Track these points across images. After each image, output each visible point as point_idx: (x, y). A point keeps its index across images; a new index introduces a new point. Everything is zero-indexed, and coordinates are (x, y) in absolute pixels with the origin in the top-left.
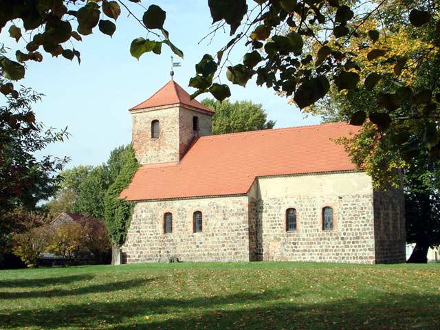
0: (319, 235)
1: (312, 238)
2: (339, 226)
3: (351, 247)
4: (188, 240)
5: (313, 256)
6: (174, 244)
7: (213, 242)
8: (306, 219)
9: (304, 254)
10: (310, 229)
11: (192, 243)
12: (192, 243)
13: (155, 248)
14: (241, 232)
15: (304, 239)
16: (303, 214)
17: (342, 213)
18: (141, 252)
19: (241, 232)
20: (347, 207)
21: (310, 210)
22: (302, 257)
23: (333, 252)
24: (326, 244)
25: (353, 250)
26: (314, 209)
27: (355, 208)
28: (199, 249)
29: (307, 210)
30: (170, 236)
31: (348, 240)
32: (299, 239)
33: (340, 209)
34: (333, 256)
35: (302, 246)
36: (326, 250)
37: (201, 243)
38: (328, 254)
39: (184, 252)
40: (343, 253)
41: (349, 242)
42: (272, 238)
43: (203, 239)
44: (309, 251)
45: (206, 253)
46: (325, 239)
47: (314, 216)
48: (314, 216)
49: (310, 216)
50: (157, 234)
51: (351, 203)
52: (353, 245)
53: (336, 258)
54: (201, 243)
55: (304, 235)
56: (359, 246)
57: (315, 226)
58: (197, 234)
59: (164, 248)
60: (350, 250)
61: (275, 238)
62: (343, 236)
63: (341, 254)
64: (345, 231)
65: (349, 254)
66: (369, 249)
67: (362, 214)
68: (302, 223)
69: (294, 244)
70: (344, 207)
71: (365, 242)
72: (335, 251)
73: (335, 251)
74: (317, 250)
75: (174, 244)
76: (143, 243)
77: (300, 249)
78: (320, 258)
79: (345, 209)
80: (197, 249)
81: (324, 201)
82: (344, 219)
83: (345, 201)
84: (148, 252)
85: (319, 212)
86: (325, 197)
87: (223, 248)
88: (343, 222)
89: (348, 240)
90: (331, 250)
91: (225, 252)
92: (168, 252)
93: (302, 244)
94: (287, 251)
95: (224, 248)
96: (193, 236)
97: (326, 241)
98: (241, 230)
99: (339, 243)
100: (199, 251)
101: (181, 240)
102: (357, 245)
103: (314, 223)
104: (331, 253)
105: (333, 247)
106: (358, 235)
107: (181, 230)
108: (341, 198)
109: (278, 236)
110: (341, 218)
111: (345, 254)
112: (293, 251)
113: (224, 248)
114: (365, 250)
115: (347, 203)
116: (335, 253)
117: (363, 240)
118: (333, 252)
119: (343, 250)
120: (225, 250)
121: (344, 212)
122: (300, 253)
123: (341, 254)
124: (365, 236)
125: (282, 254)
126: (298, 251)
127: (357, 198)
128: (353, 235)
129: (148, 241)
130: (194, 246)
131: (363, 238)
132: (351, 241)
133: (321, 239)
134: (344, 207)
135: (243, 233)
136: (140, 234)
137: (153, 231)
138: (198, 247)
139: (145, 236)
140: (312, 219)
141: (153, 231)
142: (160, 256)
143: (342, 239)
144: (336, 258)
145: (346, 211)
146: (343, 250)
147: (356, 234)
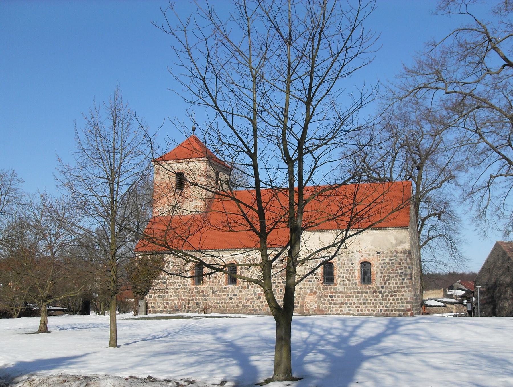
0: (357, 288)
1: (349, 292)
2: (377, 281)
3: (389, 300)
4: (220, 292)
5: (350, 309)
6: (204, 296)
7: (248, 294)
8: (344, 273)
9: (340, 307)
10: (348, 282)
11: (224, 295)
12: (224, 295)
13: (183, 300)
14: (279, 285)
15: (341, 293)
16: (340, 268)
17: (380, 268)
18: (167, 304)
19: (279, 285)
20: (385, 262)
21: (348, 264)
22: (339, 309)
23: (371, 305)
24: (364, 298)
25: (391, 303)
26: (352, 264)
27: (393, 263)
28: (232, 300)
29: (344, 264)
30: (201, 288)
31: (387, 293)
32: (336, 293)
33: (378, 264)
34: (371, 309)
35: (339, 299)
36: (364, 303)
37: (235, 295)
38: (366, 307)
39: (216, 303)
40: (381, 306)
41: (387, 296)
42: (308, 291)
43: (237, 292)
44: (347, 304)
45: (240, 305)
46: (363, 292)
47: (351, 270)
48: (351, 270)
49: (347, 270)
50: (186, 285)
51: (389, 258)
52: (391, 298)
53: (374, 311)
54: (235, 295)
55: (341, 289)
56: (397, 299)
57: (353, 280)
58: (231, 286)
59: (192, 300)
60: (387, 303)
61: (311, 291)
62: (381, 290)
63: (379, 307)
64: (383, 285)
65: (386, 307)
66: (407, 302)
67: (400, 269)
68: (339, 276)
69: (331, 296)
70: (382, 262)
71: (403, 295)
72: (373, 304)
73: (373, 304)
74: (354, 303)
75: (204, 296)
76: (169, 294)
77: (337, 302)
78: (358, 311)
79: (383, 264)
80: (231, 301)
81: (362, 256)
82: (382, 273)
83: (383, 257)
84: (175, 304)
85: (357, 267)
86: (363, 252)
87: (259, 301)
88: (381, 277)
89: (387, 293)
90: (369, 303)
91: (261, 304)
92: (197, 303)
93: (339, 297)
94: (324, 304)
95: (261, 300)
96: (225, 288)
97: (363, 295)
98: (279, 283)
99: (377, 296)
100: (232, 303)
101: (213, 292)
102: (395, 298)
103: (352, 277)
104: (368, 306)
105: (371, 300)
106: (396, 289)
107: (213, 282)
108: (378, 253)
109: (314, 290)
110: (379, 274)
111: (383, 307)
112: (330, 304)
113: (261, 300)
114: (403, 303)
115: (385, 258)
116: (373, 306)
117: (365, 306)
118: (371, 305)
119: (381, 303)
120: (261, 302)
121: (382, 267)
122: (338, 306)
123: (379, 307)
124: (403, 290)
125: (318, 306)
126: (335, 304)
127: (395, 254)
128: (390, 289)
129: (175, 292)
130: (227, 299)
131: (400, 291)
132: (371, 302)
133: (359, 293)
134: (382, 262)
135: (281, 286)
136: (167, 285)
137: (180, 282)
138: (231, 298)
139: (172, 287)
140: (350, 273)
141: (180, 282)
142: (189, 307)
143: (380, 292)
144: (374, 311)
145: (384, 265)
146: (381, 303)
147: (394, 287)
